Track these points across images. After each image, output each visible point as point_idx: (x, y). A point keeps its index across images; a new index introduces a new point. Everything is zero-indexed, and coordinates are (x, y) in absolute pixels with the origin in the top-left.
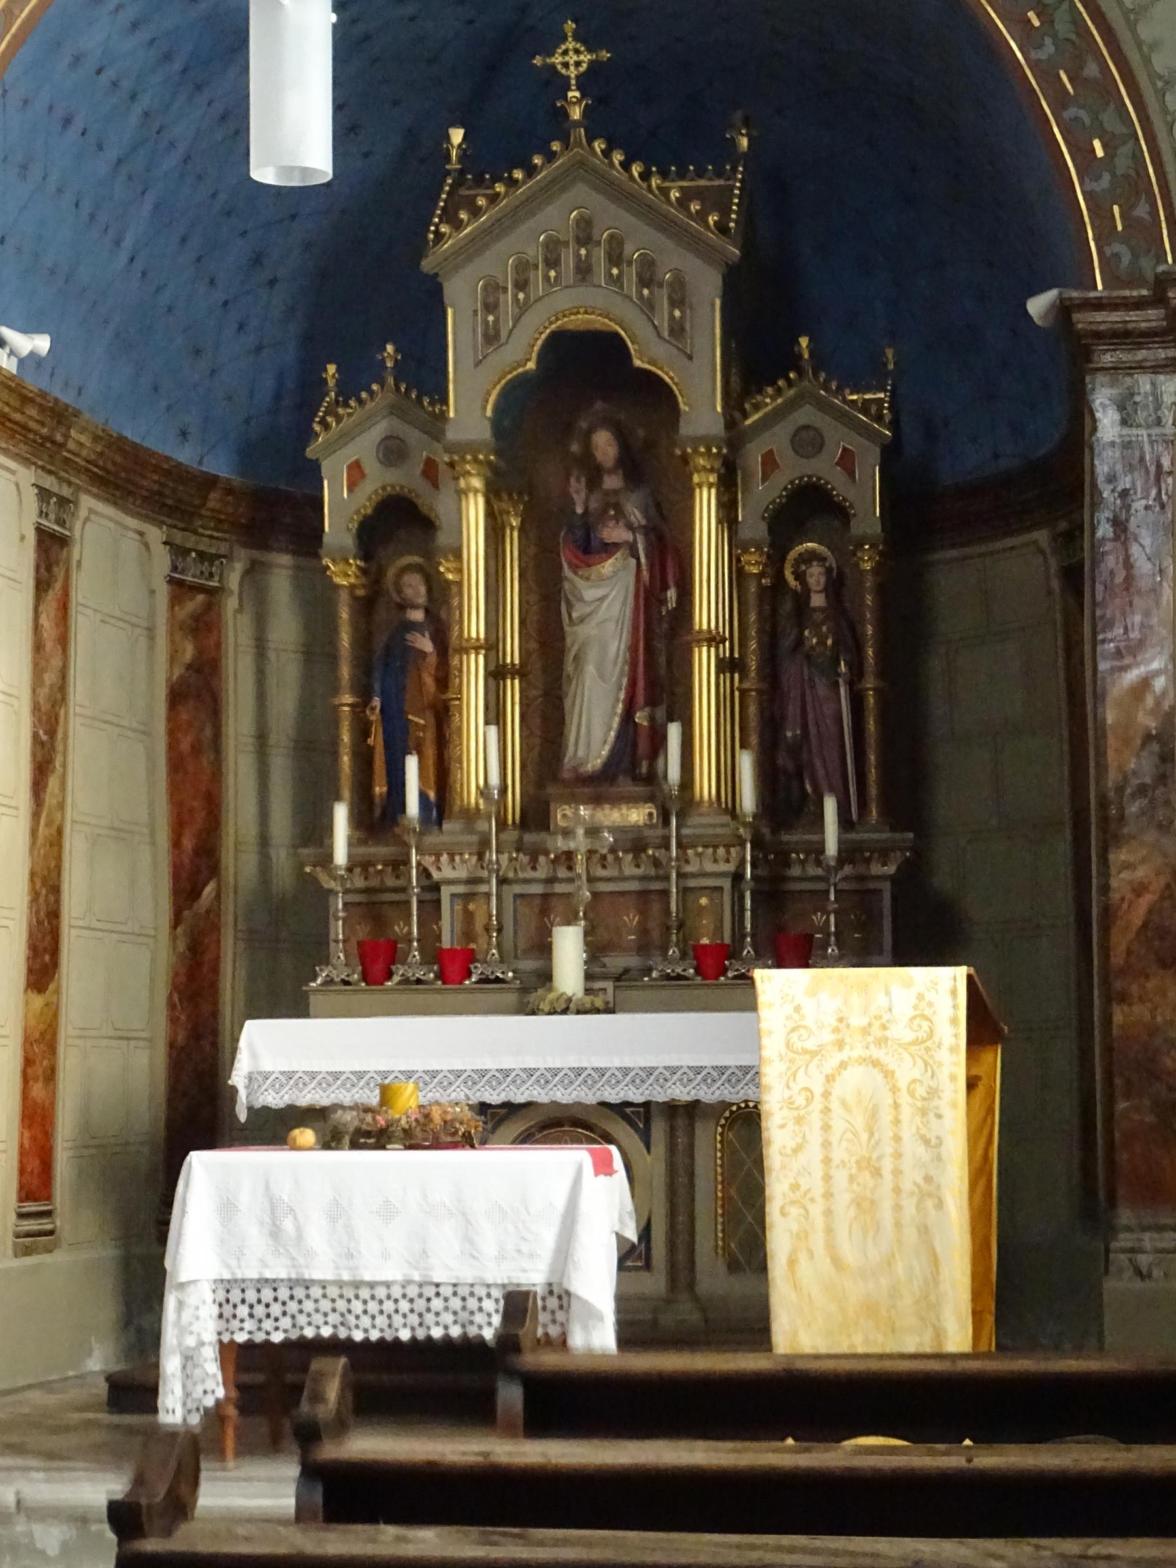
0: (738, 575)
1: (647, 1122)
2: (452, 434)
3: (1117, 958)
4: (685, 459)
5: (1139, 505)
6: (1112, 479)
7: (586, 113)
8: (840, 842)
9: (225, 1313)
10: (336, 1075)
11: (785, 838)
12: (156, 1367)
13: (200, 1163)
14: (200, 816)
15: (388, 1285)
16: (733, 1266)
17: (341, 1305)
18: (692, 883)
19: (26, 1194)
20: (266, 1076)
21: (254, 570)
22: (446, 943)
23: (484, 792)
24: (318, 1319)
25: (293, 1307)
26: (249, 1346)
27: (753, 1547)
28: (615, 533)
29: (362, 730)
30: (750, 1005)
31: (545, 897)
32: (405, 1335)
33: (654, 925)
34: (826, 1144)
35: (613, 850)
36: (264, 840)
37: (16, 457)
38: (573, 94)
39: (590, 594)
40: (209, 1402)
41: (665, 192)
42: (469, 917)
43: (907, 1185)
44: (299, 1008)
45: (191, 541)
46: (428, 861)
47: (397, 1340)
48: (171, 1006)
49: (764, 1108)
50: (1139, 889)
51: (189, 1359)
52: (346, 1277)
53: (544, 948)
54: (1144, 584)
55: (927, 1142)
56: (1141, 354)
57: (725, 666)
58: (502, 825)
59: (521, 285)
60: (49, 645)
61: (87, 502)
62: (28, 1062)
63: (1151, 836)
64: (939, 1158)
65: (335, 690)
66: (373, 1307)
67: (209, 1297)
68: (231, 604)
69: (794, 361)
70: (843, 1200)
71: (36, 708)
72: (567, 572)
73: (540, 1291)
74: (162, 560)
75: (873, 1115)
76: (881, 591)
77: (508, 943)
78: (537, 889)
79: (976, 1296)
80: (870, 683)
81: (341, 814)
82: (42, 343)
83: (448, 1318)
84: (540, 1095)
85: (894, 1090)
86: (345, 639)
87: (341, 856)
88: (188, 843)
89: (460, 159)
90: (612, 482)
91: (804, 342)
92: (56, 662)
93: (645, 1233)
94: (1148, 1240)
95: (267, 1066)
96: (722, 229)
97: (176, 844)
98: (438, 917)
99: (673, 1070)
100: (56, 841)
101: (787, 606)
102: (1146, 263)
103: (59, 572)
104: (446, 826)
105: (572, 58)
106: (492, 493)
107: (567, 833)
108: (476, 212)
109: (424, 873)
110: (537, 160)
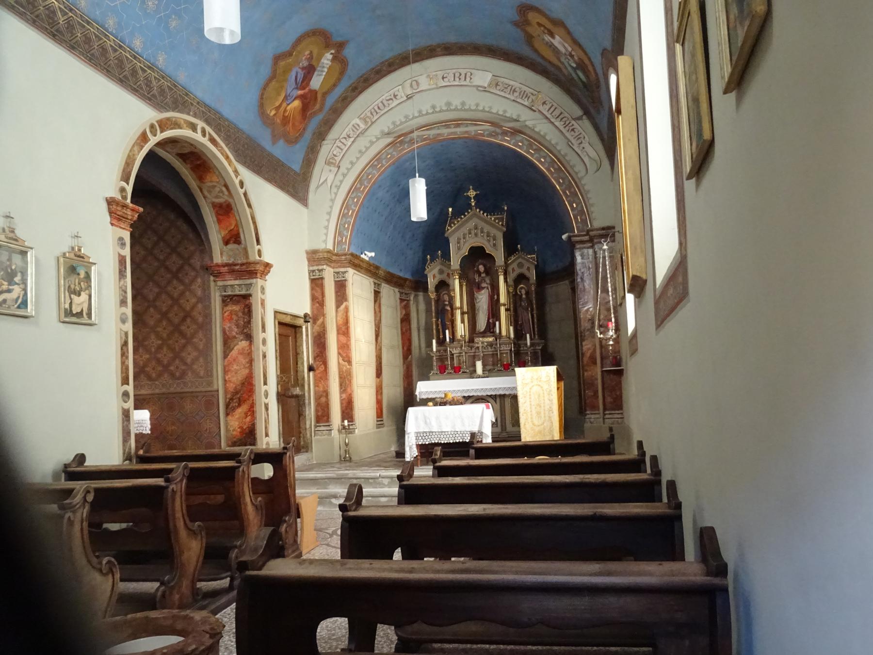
0: (508, 292)
2: (452, 268)
3: (585, 362)
4: (497, 270)
5: (585, 275)
6: (580, 270)
7: (475, 204)
8: (530, 343)
10: (436, 392)
11: (520, 342)
12: (404, 450)
13: (410, 409)
15: (448, 432)
17: (439, 436)
18: (502, 352)
19: (378, 417)
20: (422, 392)
21: (416, 296)
22: (455, 365)
23: (461, 336)
25: (430, 437)
26: (422, 444)
28: (484, 285)
29: (437, 325)
30: (515, 375)
32: (451, 442)
34: (530, 401)
35: (487, 346)
36: (420, 346)
37: (370, 277)
38: (473, 200)
39: (480, 297)
40: (415, 456)
41: (491, 218)
42: (460, 360)
43: (546, 409)
44: (428, 379)
45: (403, 291)
46: (451, 350)
49: (518, 395)
50: (589, 349)
51: (411, 448)
52: (440, 431)
53: (474, 366)
54: (587, 290)
56: (585, 245)
57: (507, 310)
58: (465, 342)
59: (464, 238)
60: (377, 312)
61: (383, 285)
62: (377, 392)
65: (432, 318)
66: (445, 436)
67: (414, 435)
68: (412, 302)
69: (517, 250)
70: (534, 412)
71: (375, 325)
72: (475, 293)
73: (477, 432)
74: (398, 295)
75: (539, 396)
78: (472, 354)
79: (560, 428)
80: (535, 312)
81: (434, 341)
82: (373, 254)
83: (460, 438)
84: (475, 394)
85: (543, 390)
86: (433, 308)
87: (434, 349)
88: (405, 348)
90: (483, 275)
91: (519, 246)
92: (379, 315)
93: (496, 420)
94: (593, 416)
96: (502, 225)
98: (453, 360)
99: (500, 388)
100: (380, 349)
102: (585, 227)
105: (472, 193)
106: (460, 278)
107: (478, 343)
108: (455, 224)
109: (451, 352)
110: (466, 214)
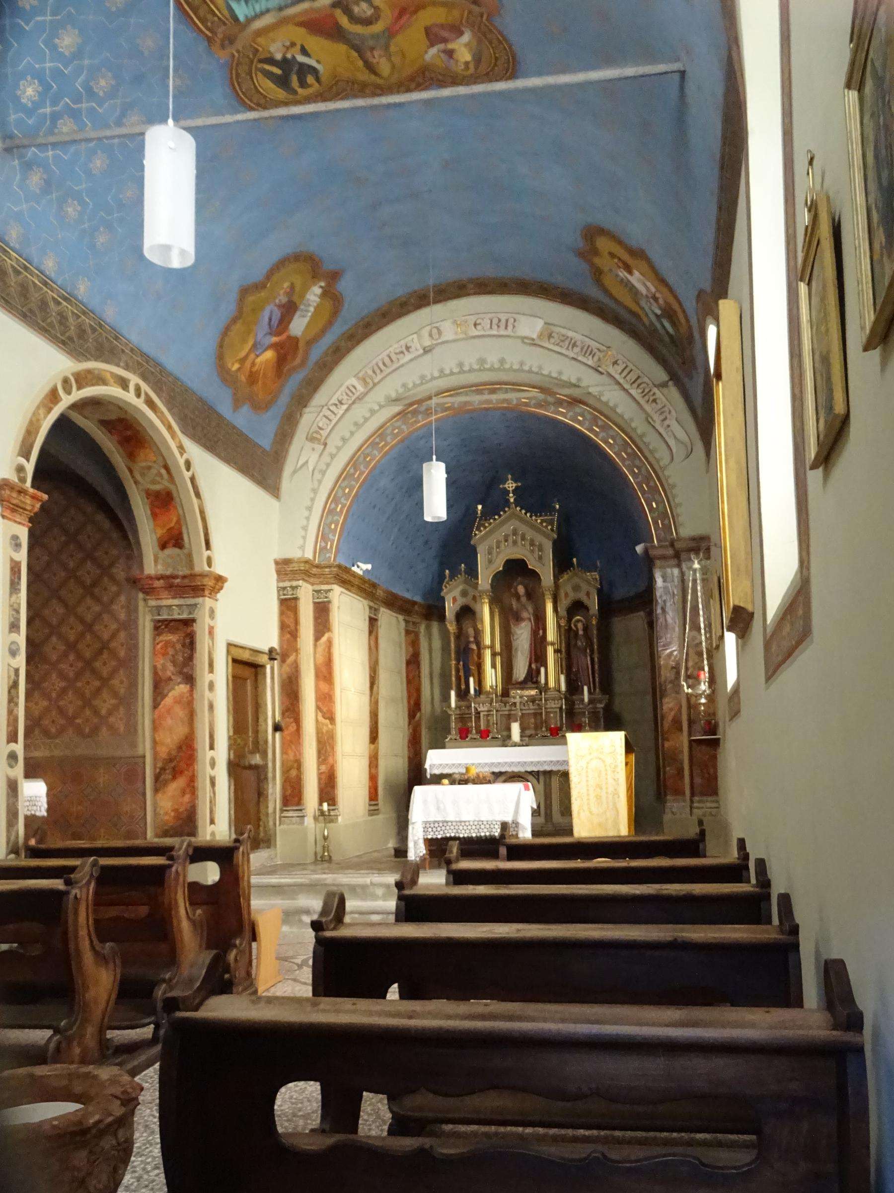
1: (538, 776)
6: (661, 597)
7: (515, 499)
9: (425, 831)
11: (574, 697)
12: (406, 845)
13: (417, 789)
14: (415, 695)
15: (469, 821)
16: (563, 814)
17: (456, 827)
18: (549, 710)
19: (371, 799)
20: (434, 765)
23: (491, 687)
24: (450, 831)
25: (443, 828)
26: (432, 839)
27: (569, 888)
29: (458, 671)
30: (565, 743)
31: (509, 715)
32: (474, 835)
33: (539, 721)
35: (527, 702)
38: (511, 495)
40: (421, 854)
41: (536, 520)
42: (488, 721)
44: (443, 747)
45: (410, 619)
46: (477, 706)
47: (472, 837)
48: (409, 747)
50: (671, 709)
51: (416, 843)
52: (458, 820)
53: (509, 729)
55: (614, 780)
57: (556, 651)
58: (496, 695)
59: (498, 547)
61: (382, 610)
63: (674, 695)
64: (618, 784)
65: (451, 660)
67: (421, 826)
69: (572, 565)
71: (370, 667)
72: (512, 626)
73: (510, 822)
76: (598, 630)
77: (499, 728)
78: (507, 713)
81: (453, 694)
82: (369, 567)
84: (509, 769)
85: (605, 766)
86: (453, 646)
87: (453, 705)
88: (412, 703)
89: (481, 513)
90: (524, 599)
91: (575, 560)
93: (539, 806)
95: (434, 763)
96: (552, 530)
97: (409, 702)
100: (377, 703)
101: (572, 634)
103: (375, 628)
104: (481, 696)
105: (510, 485)
107: (514, 698)
109: (476, 709)
110: (502, 513)
